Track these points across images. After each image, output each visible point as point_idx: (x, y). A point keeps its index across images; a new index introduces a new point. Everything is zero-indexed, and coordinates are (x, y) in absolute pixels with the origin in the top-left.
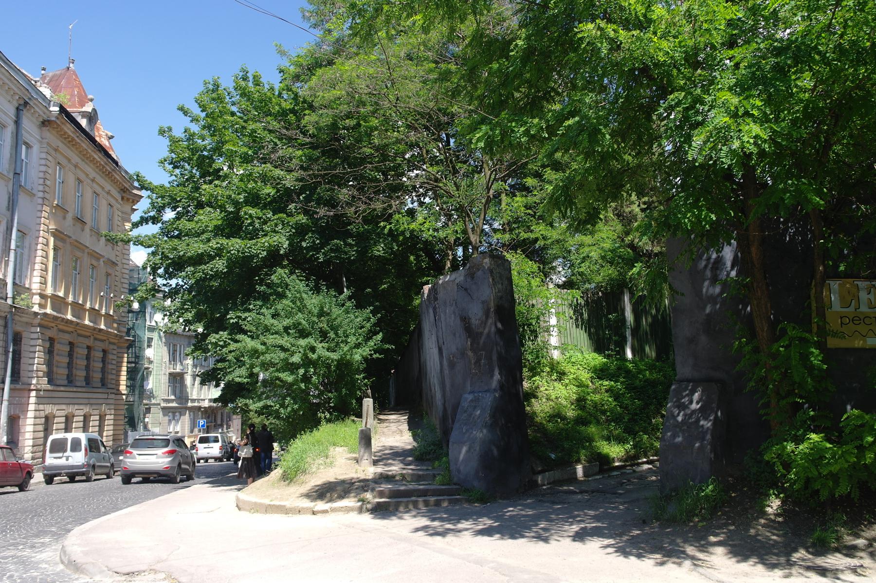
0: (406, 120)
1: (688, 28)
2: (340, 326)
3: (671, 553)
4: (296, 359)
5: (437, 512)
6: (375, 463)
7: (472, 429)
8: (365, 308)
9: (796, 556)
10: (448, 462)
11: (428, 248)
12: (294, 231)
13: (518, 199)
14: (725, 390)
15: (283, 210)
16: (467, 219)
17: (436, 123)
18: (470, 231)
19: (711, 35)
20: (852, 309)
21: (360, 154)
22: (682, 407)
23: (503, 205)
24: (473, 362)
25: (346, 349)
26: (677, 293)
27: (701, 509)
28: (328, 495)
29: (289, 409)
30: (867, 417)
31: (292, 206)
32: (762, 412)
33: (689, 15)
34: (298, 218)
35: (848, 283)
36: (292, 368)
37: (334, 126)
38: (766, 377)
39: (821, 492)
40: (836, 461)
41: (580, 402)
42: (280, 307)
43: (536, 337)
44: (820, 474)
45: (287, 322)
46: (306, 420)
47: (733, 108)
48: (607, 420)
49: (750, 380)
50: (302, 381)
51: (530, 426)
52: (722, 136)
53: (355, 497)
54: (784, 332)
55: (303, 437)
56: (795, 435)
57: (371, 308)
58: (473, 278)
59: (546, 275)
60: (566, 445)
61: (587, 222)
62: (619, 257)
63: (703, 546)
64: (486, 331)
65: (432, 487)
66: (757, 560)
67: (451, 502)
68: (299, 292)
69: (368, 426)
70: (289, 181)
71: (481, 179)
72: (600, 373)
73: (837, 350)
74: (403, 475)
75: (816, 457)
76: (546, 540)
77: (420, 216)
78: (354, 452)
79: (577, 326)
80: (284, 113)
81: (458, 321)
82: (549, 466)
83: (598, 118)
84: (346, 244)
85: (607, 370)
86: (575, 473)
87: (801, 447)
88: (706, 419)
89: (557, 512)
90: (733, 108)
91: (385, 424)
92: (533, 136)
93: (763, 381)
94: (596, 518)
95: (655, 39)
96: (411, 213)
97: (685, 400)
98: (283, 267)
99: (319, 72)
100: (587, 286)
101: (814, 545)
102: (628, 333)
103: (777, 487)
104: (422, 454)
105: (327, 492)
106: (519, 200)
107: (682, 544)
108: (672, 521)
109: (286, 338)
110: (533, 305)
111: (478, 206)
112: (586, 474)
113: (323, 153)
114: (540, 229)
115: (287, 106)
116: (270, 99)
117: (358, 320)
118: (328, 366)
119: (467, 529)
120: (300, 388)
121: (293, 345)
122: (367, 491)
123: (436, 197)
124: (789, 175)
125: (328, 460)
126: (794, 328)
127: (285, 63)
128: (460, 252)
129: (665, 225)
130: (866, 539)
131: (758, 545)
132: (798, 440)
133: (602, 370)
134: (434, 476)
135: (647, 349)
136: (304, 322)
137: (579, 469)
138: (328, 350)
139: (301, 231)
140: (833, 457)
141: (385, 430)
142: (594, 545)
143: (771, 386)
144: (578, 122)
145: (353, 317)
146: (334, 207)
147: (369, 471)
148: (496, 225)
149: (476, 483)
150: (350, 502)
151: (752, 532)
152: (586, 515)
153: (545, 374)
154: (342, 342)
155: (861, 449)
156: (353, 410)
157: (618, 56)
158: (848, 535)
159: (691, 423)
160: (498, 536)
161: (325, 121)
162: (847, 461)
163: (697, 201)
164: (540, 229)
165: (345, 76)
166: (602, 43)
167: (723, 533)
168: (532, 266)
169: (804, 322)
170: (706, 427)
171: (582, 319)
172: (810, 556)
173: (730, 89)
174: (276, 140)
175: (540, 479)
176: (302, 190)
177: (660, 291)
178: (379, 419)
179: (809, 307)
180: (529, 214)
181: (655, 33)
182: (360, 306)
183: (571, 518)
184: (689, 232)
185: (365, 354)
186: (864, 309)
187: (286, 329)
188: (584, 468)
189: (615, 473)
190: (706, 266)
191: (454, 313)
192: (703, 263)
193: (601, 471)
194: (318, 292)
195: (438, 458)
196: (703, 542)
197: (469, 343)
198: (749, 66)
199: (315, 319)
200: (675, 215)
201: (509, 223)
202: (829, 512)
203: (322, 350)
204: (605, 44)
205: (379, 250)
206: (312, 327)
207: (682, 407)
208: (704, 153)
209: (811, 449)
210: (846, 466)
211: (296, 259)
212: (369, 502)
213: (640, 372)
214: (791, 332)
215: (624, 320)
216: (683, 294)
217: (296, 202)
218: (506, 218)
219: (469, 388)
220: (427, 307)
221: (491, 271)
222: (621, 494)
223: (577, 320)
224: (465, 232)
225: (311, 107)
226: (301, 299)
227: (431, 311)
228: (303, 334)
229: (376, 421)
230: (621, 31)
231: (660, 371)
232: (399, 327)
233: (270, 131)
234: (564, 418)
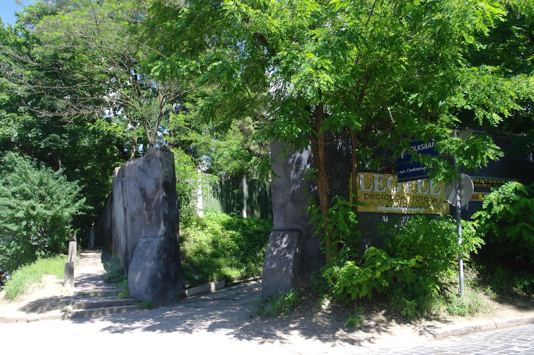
0: (107, 57)
1: (289, 13)
2: (55, 192)
3: (269, 336)
4: (21, 214)
5: (119, 317)
6: (76, 285)
7: (144, 261)
8: (73, 181)
9: (338, 333)
10: (127, 283)
11: (120, 144)
12: (22, 125)
13: (180, 115)
14: (302, 236)
15: (15, 111)
16: (147, 126)
17: (126, 62)
18: (148, 134)
19: (303, 19)
20: (370, 190)
21: (74, 78)
22: (276, 246)
23: (171, 119)
24: (147, 217)
25: (58, 208)
26: (277, 176)
27: (285, 308)
28: (40, 309)
29: (14, 249)
30: (378, 251)
31: (22, 108)
32: (322, 249)
33: (292, 6)
34: (26, 117)
35: (370, 175)
36: (17, 221)
37: (55, 56)
38: (324, 228)
39: (352, 295)
40: (361, 277)
41: (214, 243)
42: (9, 178)
43: (189, 202)
44: (352, 284)
45: (14, 189)
46: (27, 256)
47: (314, 64)
48: (231, 255)
49: (316, 230)
50: (24, 230)
51: (183, 259)
52: (309, 79)
53: (60, 309)
54: (336, 201)
55: (23, 268)
56: (339, 262)
57: (78, 181)
58: (149, 163)
59: (196, 164)
60: (206, 270)
61: (223, 129)
62: (241, 155)
63: (286, 330)
64: (156, 198)
65: (116, 300)
66: (316, 337)
67: (128, 309)
68: (24, 168)
69: (72, 261)
70: (21, 91)
71: (157, 101)
72: (228, 226)
73: (362, 213)
74: (96, 294)
75: (350, 275)
76: (190, 332)
77: (113, 121)
78: (61, 278)
79: (214, 197)
80: (18, 45)
81: (138, 191)
82: (194, 284)
83: (234, 63)
84: (61, 138)
85: (232, 224)
86: (210, 288)
87: (342, 269)
88: (290, 253)
89: (198, 313)
90: (314, 64)
91: (85, 259)
92: (192, 72)
93: (322, 230)
94: (222, 316)
95: (270, 18)
96: (109, 120)
97: (278, 242)
98: (15, 151)
99: (45, 18)
100: (221, 173)
101: (347, 326)
102: (245, 202)
103: (328, 293)
104: (110, 279)
105: (37, 306)
106: (181, 116)
107: (274, 330)
108: (268, 316)
109: (13, 200)
110: (187, 183)
111: (154, 119)
112: (217, 289)
113: (47, 74)
114: (193, 136)
115: (21, 39)
116: (8, 34)
117: (68, 189)
118: (45, 220)
119: (138, 328)
120: (22, 235)
121: (18, 205)
122: (68, 304)
123: (126, 110)
124: (342, 109)
125: (41, 284)
126: (341, 199)
127: (20, 10)
128: (141, 147)
129: (271, 132)
130: (375, 321)
131: (317, 328)
132: (341, 265)
133: (228, 224)
134: (118, 293)
135: (256, 212)
136: (27, 189)
137: (213, 286)
138: (45, 209)
139: (27, 127)
140: (359, 274)
141: (85, 263)
142: (222, 332)
143: (327, 234)
144: (221, 64)
145: (64, 187)
146: (53, 111)
147: (70, 290)
148: (166, 132)
149: (146, 297)
150: (57, 312)
151: (314, 320)
152: (216, 314)
153: (193, 226)
154: (55, 203)
155: (374, 269)
156: (62, 250)
157: (247, 26)
158: (366, 319)
159: (282, 256)
160: (159, 331)
161: (49, 52)
162: (367, 277)
163: (291, 120)
164: (193, 136)
165: (64, 23)
166: (238, 15)
167: (298, 322)
168: (187, 158)
169: (346, 196)
170: (289, 258)
171: (218, 193)
172: (346, 333)
173: (312, 52)
174: (12, 63)
175: (187, 292)
176: (30, 98)
177: (267, 175)
178: (81, 256)
179: (349, 188)
180: (187, 125)
181: (270, 15)
182: (70, 179)
183: (207, 317)
184: (285, 139)
185: (72, 212)
186: (376, 190)
187: (14, 194)
188: (216, 284)
189: (234, 287)
190: (293, 162)
191: (135, 185)
192: (291, 160)
193: (226, 286)
194: (39, 169)
195: (120, 281)
196: (286, 328)
197: (145, 205)
198: (324, 40)
199: (36, 187)
200: (278, 128)
201: (174, 131)
202: (356, 306)
203: (40, 208)
204: (240, 16)
205: (85, 142)
206: (34, 193)
207: (276, 246)
208: (297, 89)
209: (348, 270)
210: (366, 279)
211: (25, 147)
212: (70, 312)
213: (251, 225)
214: (340, 202)
215: (242, 194)
216: (280, 177)
217: (24, 106)
218: (172, 127)
219: (143, 235)
220: (117, 182)
221: (161, 159)
222: (238, 300)
223: (214, 193)
224: (145, 134)
225: (39, 42)
226: (26, 173)
227: (120, 184)
228: (27, 197)
229: (79, 257)
230: (250, 9)
231: (262, 225)
232: (97, 194)
233: (7, 55)
234: (205, 254)
